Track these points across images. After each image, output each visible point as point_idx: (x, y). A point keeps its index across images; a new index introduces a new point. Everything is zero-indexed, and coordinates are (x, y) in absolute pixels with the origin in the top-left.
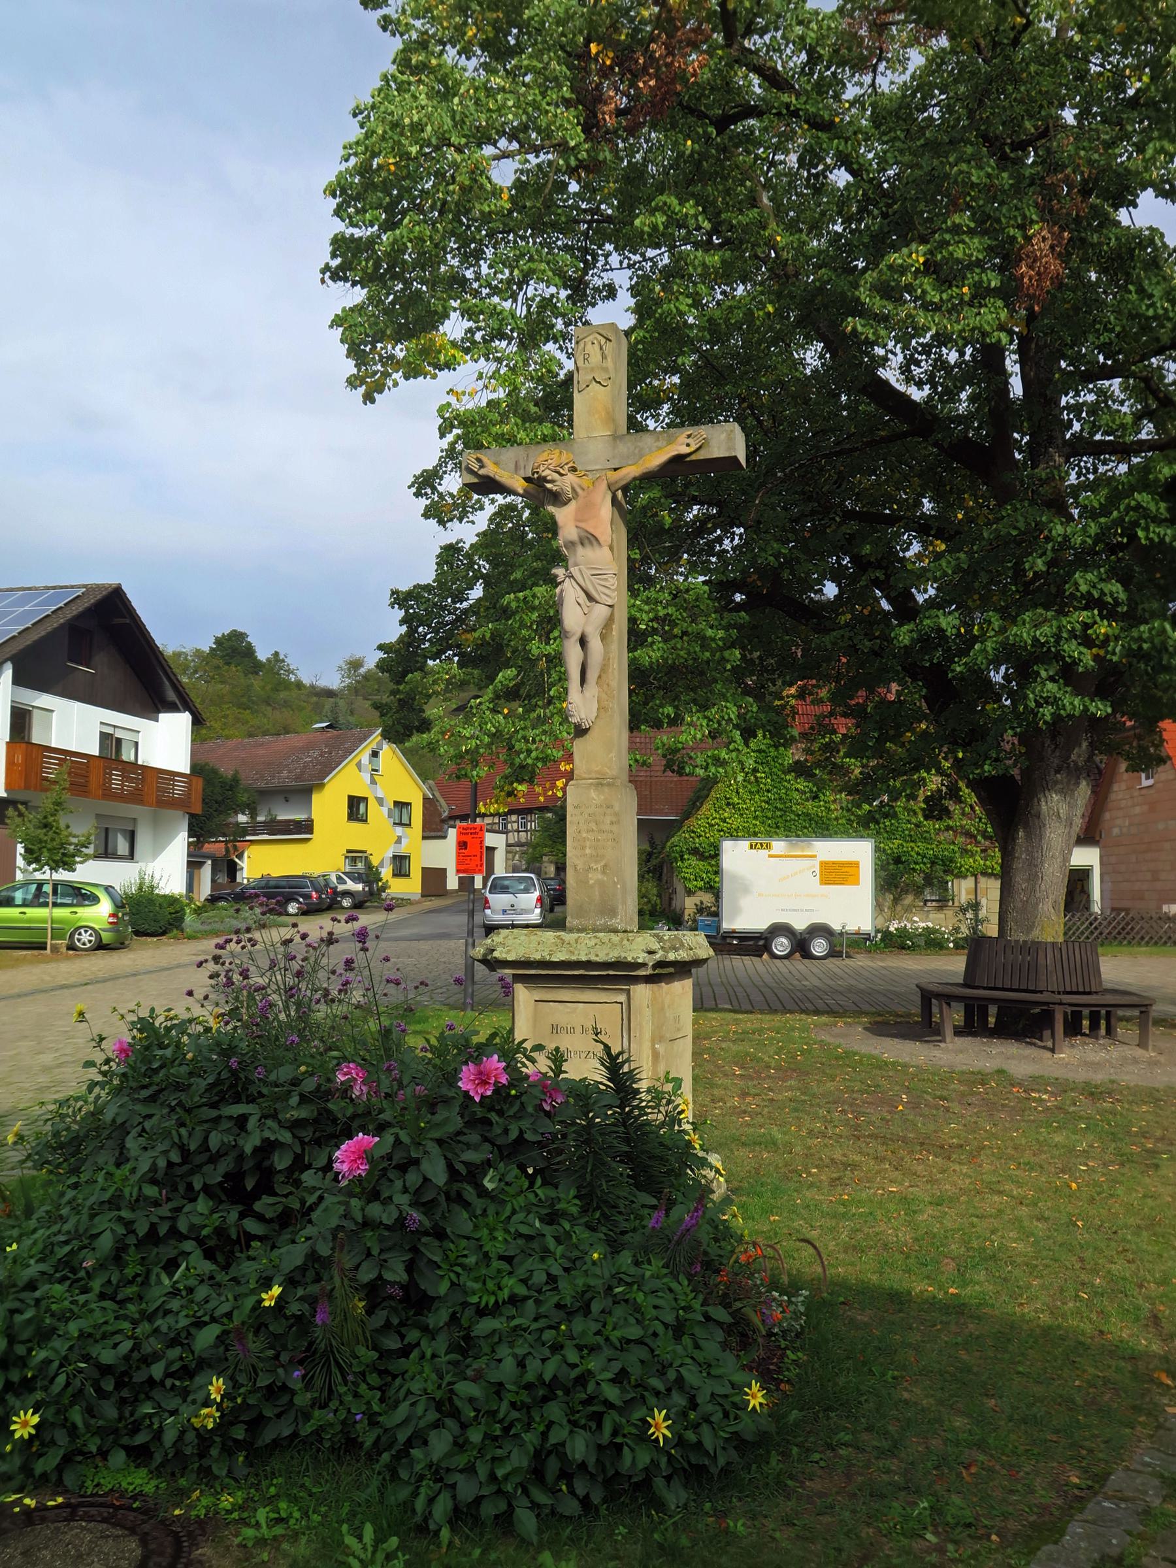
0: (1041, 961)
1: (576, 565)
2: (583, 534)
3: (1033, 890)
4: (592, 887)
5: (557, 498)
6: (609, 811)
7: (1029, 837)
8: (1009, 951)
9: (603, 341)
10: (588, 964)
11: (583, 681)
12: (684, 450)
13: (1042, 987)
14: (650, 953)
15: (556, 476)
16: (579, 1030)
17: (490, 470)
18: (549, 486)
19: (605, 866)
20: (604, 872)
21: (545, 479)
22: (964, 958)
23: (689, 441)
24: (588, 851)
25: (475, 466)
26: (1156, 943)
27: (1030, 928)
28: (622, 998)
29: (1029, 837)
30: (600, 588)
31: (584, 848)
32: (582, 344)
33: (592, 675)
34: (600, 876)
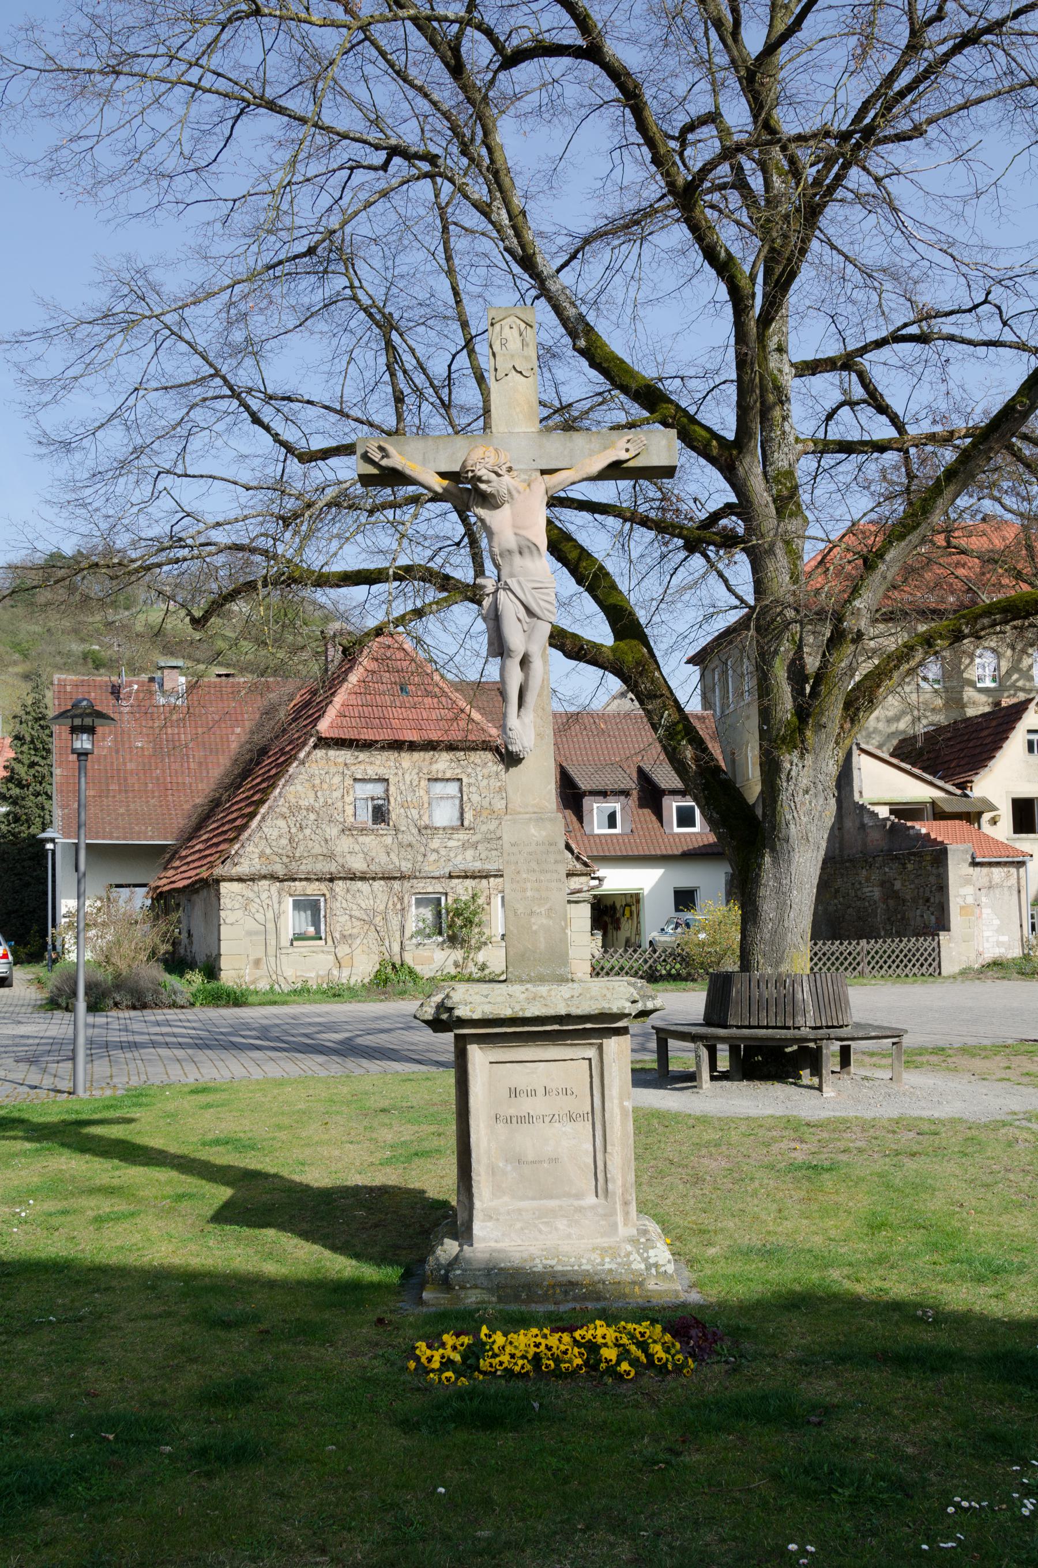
0: (799, 996)
1: (512, 575)
2: (524, 543)
3: (781, 920)
4: (535, 932)
5: (488, 500)
6: (552, 849)
7: (776, 861)
8: (762, 985)
9: (523, 325)
10: (567, 1019)
11: (520, 705)
12: (624, 456)
13: (790, 1023)
14: (634, 1002)
15: (493, 476)
16: (541, 1091)
17: (397, 460)
18: (483, 486)
19: (550, 909)
20: (549, 917)
21: (480, 479)
22: (703, 995)
23: (628, 446)
24: (529, 894)
25: (376, 456)
26: (608, 974)
27: (778, 963)
28: (591, 1053)
29: (776, 861)
30: (542, 603)
31: (524, 890)
32: (497, 326)
33: (531, 698)
34: (545, 921)
